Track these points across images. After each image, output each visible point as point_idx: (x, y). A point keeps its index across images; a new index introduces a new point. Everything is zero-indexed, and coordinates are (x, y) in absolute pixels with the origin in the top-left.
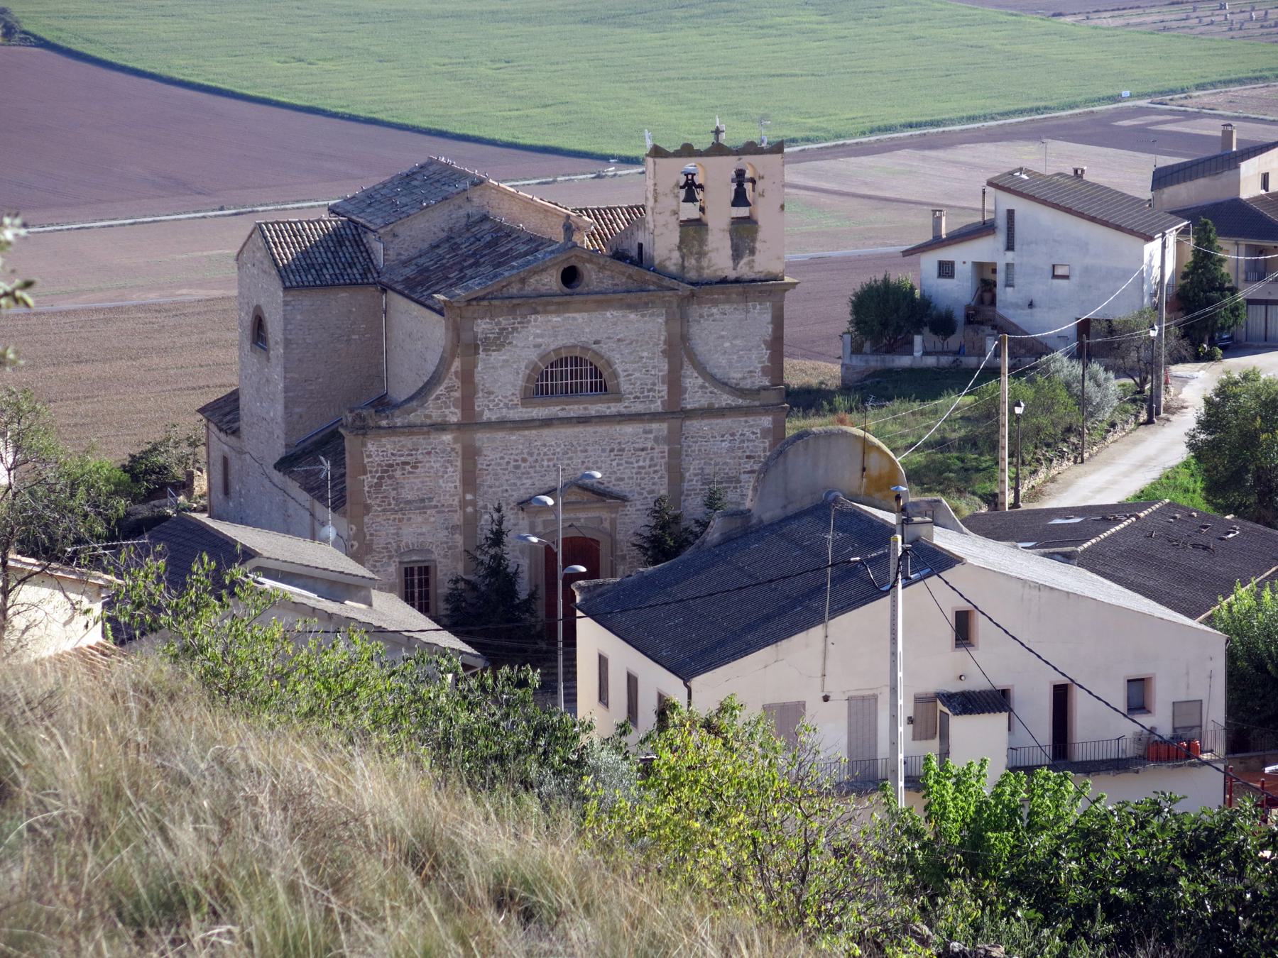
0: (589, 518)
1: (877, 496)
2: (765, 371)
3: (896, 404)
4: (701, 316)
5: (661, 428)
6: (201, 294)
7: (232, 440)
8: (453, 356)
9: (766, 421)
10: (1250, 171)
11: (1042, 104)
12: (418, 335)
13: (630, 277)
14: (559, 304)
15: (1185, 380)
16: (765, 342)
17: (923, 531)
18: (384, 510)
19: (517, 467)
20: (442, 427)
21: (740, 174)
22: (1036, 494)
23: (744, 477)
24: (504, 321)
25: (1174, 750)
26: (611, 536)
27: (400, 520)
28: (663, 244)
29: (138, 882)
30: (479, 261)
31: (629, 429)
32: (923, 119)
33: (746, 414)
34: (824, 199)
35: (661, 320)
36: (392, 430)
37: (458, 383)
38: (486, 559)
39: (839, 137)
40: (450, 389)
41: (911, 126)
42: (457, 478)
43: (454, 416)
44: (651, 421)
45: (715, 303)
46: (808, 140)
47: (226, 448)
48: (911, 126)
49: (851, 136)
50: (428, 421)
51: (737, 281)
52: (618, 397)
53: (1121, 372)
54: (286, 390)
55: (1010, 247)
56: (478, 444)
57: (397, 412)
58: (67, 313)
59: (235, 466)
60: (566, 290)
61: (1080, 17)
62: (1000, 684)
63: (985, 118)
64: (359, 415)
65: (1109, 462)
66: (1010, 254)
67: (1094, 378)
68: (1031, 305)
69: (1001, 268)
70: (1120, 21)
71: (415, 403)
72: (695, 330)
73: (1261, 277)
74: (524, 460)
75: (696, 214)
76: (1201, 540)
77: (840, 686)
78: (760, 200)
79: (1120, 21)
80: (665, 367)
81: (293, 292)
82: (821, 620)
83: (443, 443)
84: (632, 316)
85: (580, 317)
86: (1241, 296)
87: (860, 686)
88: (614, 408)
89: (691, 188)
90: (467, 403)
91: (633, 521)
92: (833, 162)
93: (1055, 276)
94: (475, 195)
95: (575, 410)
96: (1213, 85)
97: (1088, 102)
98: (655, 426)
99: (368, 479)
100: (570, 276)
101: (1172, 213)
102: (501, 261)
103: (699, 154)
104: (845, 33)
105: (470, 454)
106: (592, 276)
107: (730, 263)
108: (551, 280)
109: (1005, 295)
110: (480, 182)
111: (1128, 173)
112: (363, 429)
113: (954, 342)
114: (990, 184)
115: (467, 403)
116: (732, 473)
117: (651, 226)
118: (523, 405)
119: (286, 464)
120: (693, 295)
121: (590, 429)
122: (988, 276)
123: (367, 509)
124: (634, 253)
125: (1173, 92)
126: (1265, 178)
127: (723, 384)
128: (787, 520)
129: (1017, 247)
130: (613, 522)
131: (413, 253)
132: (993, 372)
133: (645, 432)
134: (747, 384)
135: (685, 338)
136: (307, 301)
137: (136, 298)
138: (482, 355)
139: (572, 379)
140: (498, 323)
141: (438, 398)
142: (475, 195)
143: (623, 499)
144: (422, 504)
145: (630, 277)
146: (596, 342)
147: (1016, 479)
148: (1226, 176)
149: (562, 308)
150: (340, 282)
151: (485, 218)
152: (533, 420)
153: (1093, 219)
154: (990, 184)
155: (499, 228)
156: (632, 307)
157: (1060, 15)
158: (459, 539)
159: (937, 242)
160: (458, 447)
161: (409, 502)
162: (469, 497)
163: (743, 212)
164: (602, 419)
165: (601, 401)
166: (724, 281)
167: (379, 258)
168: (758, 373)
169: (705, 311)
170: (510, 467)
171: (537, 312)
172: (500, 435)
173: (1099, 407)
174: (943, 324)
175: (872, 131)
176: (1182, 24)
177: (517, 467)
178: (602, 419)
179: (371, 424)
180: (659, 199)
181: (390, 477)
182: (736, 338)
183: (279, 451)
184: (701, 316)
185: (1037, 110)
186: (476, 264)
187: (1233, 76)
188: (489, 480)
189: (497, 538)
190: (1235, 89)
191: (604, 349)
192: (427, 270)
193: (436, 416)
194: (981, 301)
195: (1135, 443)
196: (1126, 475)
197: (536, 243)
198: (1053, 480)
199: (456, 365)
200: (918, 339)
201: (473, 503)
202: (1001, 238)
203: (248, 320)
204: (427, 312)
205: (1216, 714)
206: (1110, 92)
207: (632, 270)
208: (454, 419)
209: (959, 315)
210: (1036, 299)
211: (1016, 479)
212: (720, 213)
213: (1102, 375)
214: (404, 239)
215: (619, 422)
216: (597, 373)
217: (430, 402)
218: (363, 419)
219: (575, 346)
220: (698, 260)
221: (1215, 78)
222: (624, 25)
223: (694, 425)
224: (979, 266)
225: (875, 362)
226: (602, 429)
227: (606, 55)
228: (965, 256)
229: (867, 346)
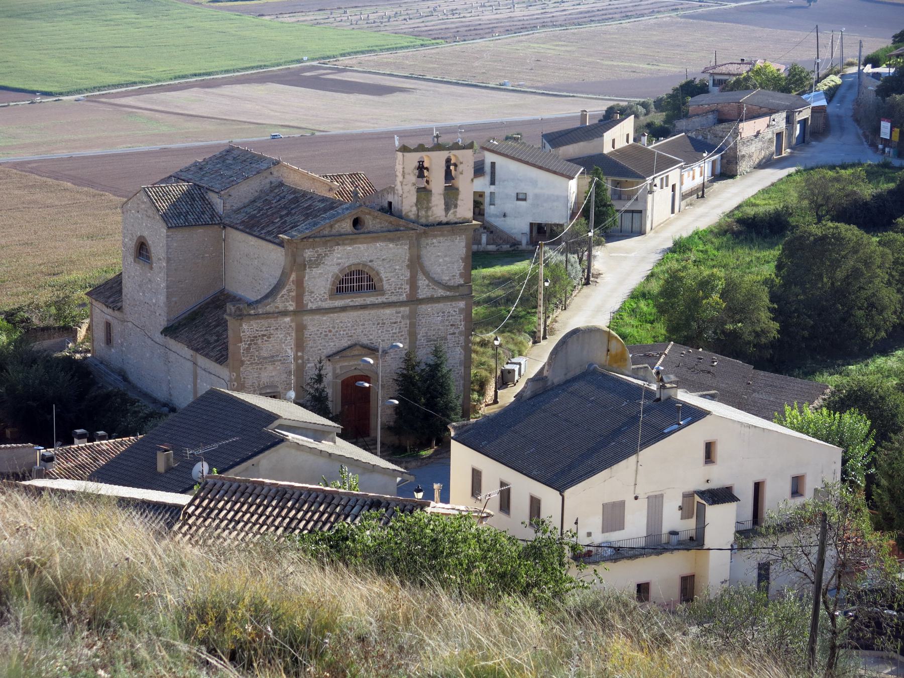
1: (615, 365)
2: (461, 275)
4: (427, 244)
5: (405, 310)
7: (117, 313)
8: (292, 271)
11: (263, 64)
12: (254, 261)
13: (391, 222)
14: (351, 239)
16: (462, 258)
18: (251, 364)
19: (326, 335)
20: (285, 313)
21: (448, 161)
23: (449, 337)
24: (320, 250)
27: (260, 369)
29: (59, 572)
30: (284, 213)
32: (202, 71)
33: (451, 301)
34: (158, 115)
35: (406, 247)
36: (257, 316)
37: (294, 287)
38: (312, 391)
39: (158, 81)
40: (290, 291)
41: (195, 75)
42: (293, 343)
43: (291, 306)
44: (400, 306)
45: (435, 236)
46: (142, 83)
47: (109, 317)
48: (195, 75)
49: (165, 81)
50: (277, 310)
51: (447, 223)
52: (382, 292)
54: (168, 287)
55: (493, 183)
56: (305, 323)
57: (260, 306)
59: (117, 329)
60: (356, 231)
61: (273, 17)
62: (727, 483)
63: (234, 71)
64: (238, 308)
66: (492, 187)
68: (505, 216)
69: (487, 195)
70: (293, 19)
71: (270, 300)
72: (423, 252)
74: (330, 331)
75: (424, 184)
77: (644, 490)
78: (461, 176)
79: (293, 19)
81: (172, 230)
82: (635, 452)
83: (284, 322)
84: (391, 245)
85: (363, 247)
87: (653, 490)
88: (380, 299)
89: (421, 169)
90: (299, 299)
92: (158, 95)
93: (518, 199)
94: (274, 170)
96: (349, 54)
97: (286, 63)
98: (402, 309)
99: (243, 346)
100: (356, 222)
101: (570, 161)
104: (151, 24)
105: (300, 329)
106: (370, 222)
107: (443, 213)
108: (346, 226)
109: (490, 210)
110: (277, 163)
115: (299, 299)
116: (443, 335)
117: (400, 192)
118: (330, 299)
119: (170, 331)
120: (425, 233)
121: (367, 312)
122: (480, 199)
123: (242, 363)
124: (386, 205)
125: (329, 57)
127: (438, 283)
129: (496, 183)
131: (240, 205)
133: (397, 313)
134: (451, 283)
135: (419, 257)
136: (180, 235)
138: (308, 270)
140: (317, 252)
141: (282, 296)
142: (274, 170)
144: (272, 359)
145: (391, 222)
146: (371, 261)
148: (596, 141)
149: (353, 242)
150: (199, 223)
151: (281, 184)
152: (336, 308)
156: (391, 240)
157: (262, 15)
160: (293, 325)
161: (265, 358)
162: (299, 354)
165: (373, 296)
168: (458, 276)
169: (429, 241)
170: (322, 336)
171: (338, 244)
172: (317, 317)
175: (176, 78)
176: (326, 21)
177: (326, 335)
179: (245, 313)
180: (406, 176)
181: (255, 344)
182: (446, 256)
183: (163, 322)
184: (427, 244)
187: (358, 49)
188: (311, 344)
189: (320, 378)
190: (361, 57)
191: (375, 265)
192: (254, 216)
197: (331, 205)
199: (293, 276)
201: (302, 358)
203: (132, 244)
206: (296, 58)
208: (291, 308)
210: (508, 211)
212: (438, 184)
215: (383, 308)
216: (370, 279)
218: (240, 310)
219: (359, 264)
220: (426, 212)
221: (349, 50)
222: (30, 19)
227: (25, 35)
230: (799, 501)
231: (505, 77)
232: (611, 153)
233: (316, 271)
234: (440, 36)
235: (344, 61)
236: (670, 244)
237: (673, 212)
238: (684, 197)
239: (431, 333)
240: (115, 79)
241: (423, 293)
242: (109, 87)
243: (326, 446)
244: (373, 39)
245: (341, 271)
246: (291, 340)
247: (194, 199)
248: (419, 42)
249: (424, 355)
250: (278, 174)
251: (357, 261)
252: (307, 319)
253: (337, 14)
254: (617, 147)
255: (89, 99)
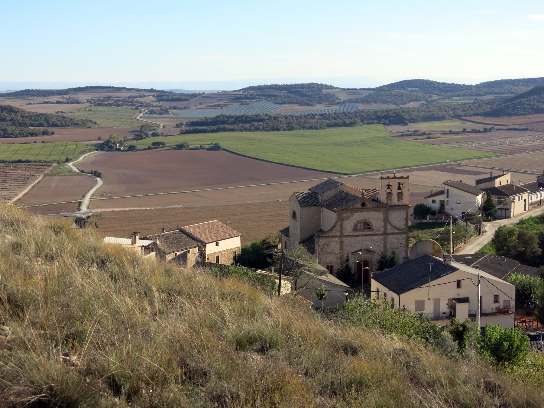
0: (368, 256)
2: (404, 225)
3: (425, 230)
5: (382, 237)
6: (259, 201)
9: (405, 236)
10: (497, 181)
12: (329, 217)
15: (485, 226)
17: (449, 262)
20: (336, 237)
21: (399, 183)
22: (457, 251)
24: (349, 214)
25: (504, 311)
26: (371, 260)
28: (383, 198)
30: (343, 201)
31: (375, 237)
36: (325, 237)
43: (338, 234)
45: (394, 210)
51: (399, 206)
53: (474, 224)
54: (301, 228)
55: (448, 197)
58: (232, 205)
59: (288, 244)
62: (467, 296)
65: (472, 243)
67: (468, 225)
69: (446, 201)
72: (389, 216)
73: (500, 204)
76: (498, 262)
80: (383, 224)
85: (365, 213)
86: (497, 208)
89: (389, 186)
90: (341, 231)
91: (376, 257)
95: (364, 233)
96: (466, 159)
100: (363, 205)
102: (348, 201)
103: (391, 178)
105: (342, 243)
106: (368, 204)
108: (359, 205)
109: (446, 207)
110: (342, 184)
111: (470, 181)
112: (319, 237)
113: (436, 217)
114: (444, 183)
115: (341, 231)
126: (500, 182)
128: (417, 259)
130: (372, 257)
131: (327, 199)
132: (449, 224)
134: (401, 228)
135: (387, 218)
136: (305, 209)
137: (246, 202)
139: (363, 226)
143: (374, 252)
144: (331, 253)
147: (453, 247)
148: (492, 182)
149: (362, 211)
150: (312, 205)
153: (466, 191)
154: (444, 183)
155: (346, 194)
156: (376, 211)
158: (339, 260)
159: (432, 196)
163: (400, 191)
164: (370, 235)
166: (396, 206)
167: (321, 200)
172: (348, 238)
173: (470, 232)
174: (433, 213)
178: (370, 235)
185: (430, 164)
186: (342, 202)
188: (346, 248)
189: (347, 260)
190: (470, 160)
191: (370, 220)
193: (334, 234)
194: (441, 208)
195: (477, 239)
196: (476, 246)
197: (355, 198)
198: (460, 247)
199: (339, 223)
200: (428, 216)
202: (445, 195)
203: (292, 213)
204: (332, 212)
205: (513, 303)
207: (376, 203)
209: (437, 211)
211: (453, 247)
212: (395, 191)
213: (470, 225)
214: (325, 196)
216: (368, 225)
217: (333, 231)
223: (389, 236)
224: (441, 201)
225: (419, 221)
226: (370, 237)
228: (438, 199)
229: (417, 218)
230: (497, 305)
231: (528, 168)
232: (499, 187)
233: (347, 222)
234: (503, 152)
235: (464, 162)
236: (518, 222)
237: (525, 209)
238: (531, 204)
239: (392, 246)
240: (372, 169)
241: (389, 231)
242: (370, 172)
243: (323, 277)
244: (476, 153)
245: (357, 222)
246: (338, 247)
247: (312, 197)
248: (495, 155)
249: (389, 254)
250: (341, 188)
251: (363, 218)
252: (344, 239)
253: (463, 144)
254: (502, 184)
255: (361, 176)
